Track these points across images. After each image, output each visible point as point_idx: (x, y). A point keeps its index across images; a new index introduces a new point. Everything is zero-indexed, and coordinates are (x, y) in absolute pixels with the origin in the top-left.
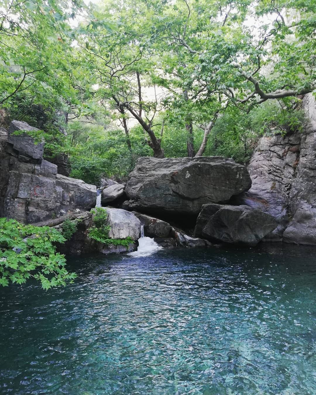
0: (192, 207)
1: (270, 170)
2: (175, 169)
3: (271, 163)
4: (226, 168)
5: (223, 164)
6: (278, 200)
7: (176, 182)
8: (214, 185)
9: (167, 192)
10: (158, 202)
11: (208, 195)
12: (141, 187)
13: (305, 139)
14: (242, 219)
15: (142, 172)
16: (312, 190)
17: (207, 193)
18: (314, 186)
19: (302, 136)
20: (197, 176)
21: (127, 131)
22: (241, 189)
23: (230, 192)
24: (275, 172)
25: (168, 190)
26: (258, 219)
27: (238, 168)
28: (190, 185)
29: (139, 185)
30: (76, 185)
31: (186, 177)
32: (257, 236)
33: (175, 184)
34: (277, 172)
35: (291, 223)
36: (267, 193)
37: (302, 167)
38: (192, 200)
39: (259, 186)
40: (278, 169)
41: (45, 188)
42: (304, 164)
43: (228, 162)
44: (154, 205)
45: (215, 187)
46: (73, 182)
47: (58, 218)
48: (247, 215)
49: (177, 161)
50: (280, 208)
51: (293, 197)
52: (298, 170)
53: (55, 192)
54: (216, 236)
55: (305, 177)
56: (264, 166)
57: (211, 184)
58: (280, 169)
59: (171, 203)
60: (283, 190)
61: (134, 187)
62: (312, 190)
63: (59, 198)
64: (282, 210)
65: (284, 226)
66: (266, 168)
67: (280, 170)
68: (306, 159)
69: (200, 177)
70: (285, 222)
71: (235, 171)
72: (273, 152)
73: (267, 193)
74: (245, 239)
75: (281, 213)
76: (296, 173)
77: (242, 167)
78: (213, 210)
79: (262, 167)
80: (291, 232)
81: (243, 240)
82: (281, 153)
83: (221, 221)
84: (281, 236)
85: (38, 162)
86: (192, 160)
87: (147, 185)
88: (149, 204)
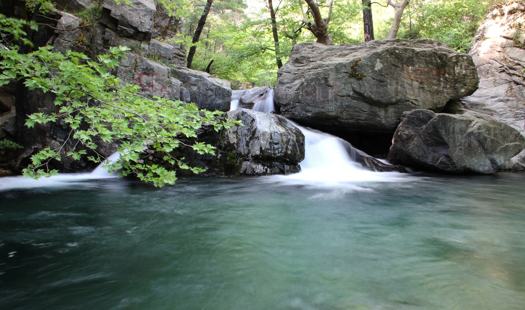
0: (385, 117)
2: (355, 57)
4: (440, 57)
5: (434, 49)
6: (518, 111)
7: (359, 78)
12: (302, 84)
15: (302, 65)
22: (463, 91)
24: (511, 68)
31: (376, 69)
34: (514, 69)
38: (385, 105)
39: (484, 91)
41: (155, 77)
43: (441, 47)
44: (324, 112)
45: (421, 86)
48: (480, 126)
49: (359, 46)
54: (429, 160)
61: (288, 85)
67: (520, 65)
69: (398, 69)
73: (501, 101)
74: (475, 165)
85: (146, 37)
87: (312, 80)
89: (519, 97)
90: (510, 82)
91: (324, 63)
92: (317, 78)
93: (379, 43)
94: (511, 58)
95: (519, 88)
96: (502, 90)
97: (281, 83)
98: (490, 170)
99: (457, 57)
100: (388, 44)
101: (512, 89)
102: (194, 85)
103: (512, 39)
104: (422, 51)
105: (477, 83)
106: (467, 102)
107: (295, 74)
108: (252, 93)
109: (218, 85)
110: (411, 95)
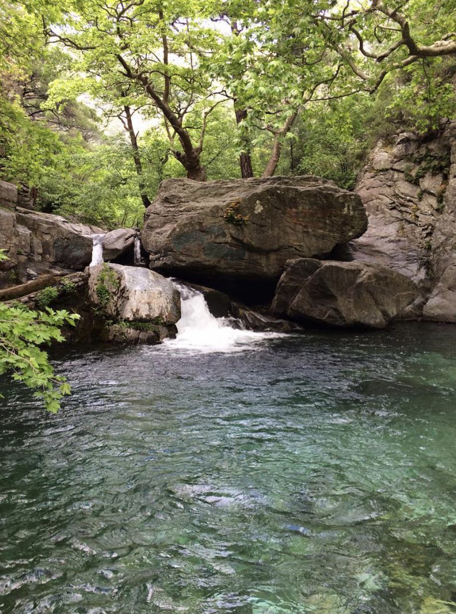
0: (267, 265)
1: (394, 203)
2: (232, 198)
4: (327, 197)
5: (320, 189)
6: (410, 253)
8: (305, 227)
12: (174, 230)
14: (361, 283)
15: (172, 205)
24: (403, 205)
25: (224, 235)
26: (385, 281)
29: (168, 228)
30: (53, 223)
31: (256, 212)
32: (385, 313)
35: (435, 292)
36: (391, 241)
40: (410, 201)
43: (326, 185)
45: (305, 230)
46: (47, 218)
50: (414, 267)
53: (17, 235)
54: (315, 314)
58: (412, 199)
61: (158, 230)
64: (419, 270)
66: (387, 200)
70: (426, 290)
71: (341, 200)
72: (398, 171)
73: (391, 241)
76: (443, 207)
79: (377, 198)
80: (437, 306)
81: (362, 321)
87: (185, 225)
89: (412, 237)
90: (402, 220)
91: (197, 205)
93: (258, 182)
94: (402, 194)
95: (412, 227)
96: (392, 230)
99: (345, 196)
101: (403, 228)
102: (46, 234)
103: (402, 172)
105: (367, 223)
108: (115, 236)
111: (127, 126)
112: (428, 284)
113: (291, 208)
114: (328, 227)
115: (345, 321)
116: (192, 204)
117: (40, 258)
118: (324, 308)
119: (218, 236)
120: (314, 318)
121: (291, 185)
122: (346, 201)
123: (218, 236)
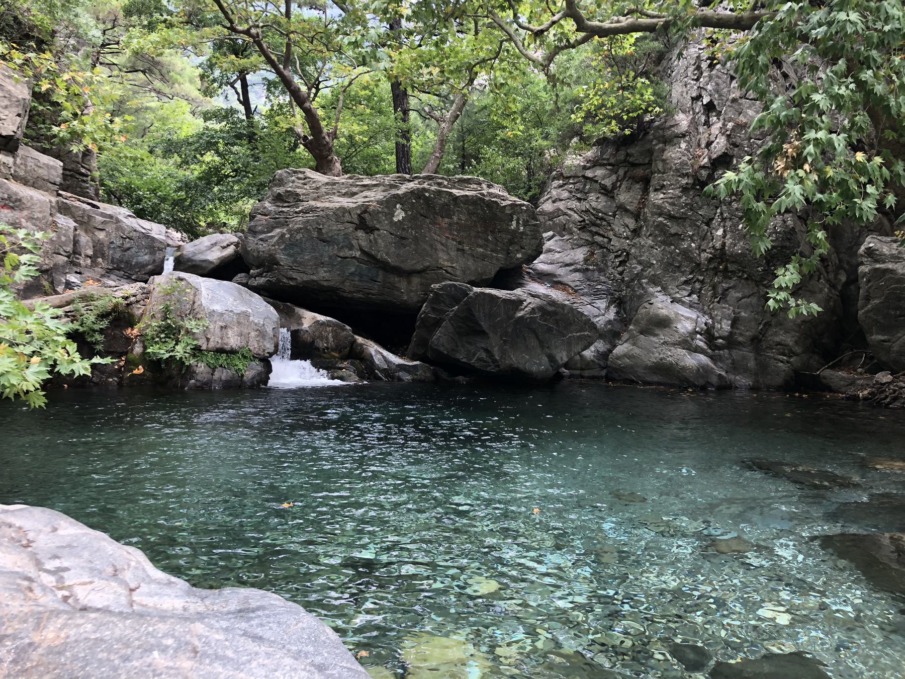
0: (407, 291)
1: (584, 221)
3: (584, 205)
6: (599, 287)
9: (347, 253)
10: (323, 275)
11: (446, 263)
12: (283, 235)
13: (663, 150)
16: (672, 265)
17: (443, 259)
18: (678, 255)
19: (656, 145)
20: (421, 218)
21: (249, 112)
22: (519, 256)
23: (494, 262)
24: (594, 224)
27: (514, 205)
28: (404, 238)
30: (111, 217)
31: (395, 219)
32: (552, 359)
33: (367, 233)
35: (625, 336)
37: (653, 214)
38: (408, 274)
39: (557, 255)
40: (602, 219)
42: (659, 207)
43: (491, 190)
44: (314, 281)
45: (460, 247)
47: (57, 293)
50: (602, 304)
51: (633, 280)
52: (645, 220)
54: (461, 357)
55: (660, 235)
56: (569, 212)
57: (453, 239)
58: (605, 217)
59: (357, 278)
60: (609, 264)
62: (672, 265)
63: (65, 244)
64: (608, 308)
65: (610, 343)
67: (605, 220)
68: (662, 196)
69: (428, 221)
70: (612, 335)
73: (576, 270)
75: (603, 315)
76: (641, 227)
77: (524, 205)
78: (458, 296)
80: (626, 355)
81: (521, 367)
82: (608, 182)
83: (470, 327)
84: (602, 363)
86: (409, 181)
87: (298, 231)
88: (300, 277)
92: (306, 228)
94: (594, 209)
95: (603, 252)
97: (253, 231)
98: (547, 369)
100: (416, 182)
104: (463, 196)
106: (533, 270)
107: (275, 218)
108: (208, 244)
109: (143, 231)
110: (444, 260)
111: (241, 99)
112: (617, 327)
113: (442, 217)
114: (490, 245)
115: (498, 366)
116: (312, 203)
117: (89, 261)
118: (472, 348)
119: (342, 247)
120: (459, 360)
121: (445, 187)
122: (514, 213)
123: (342, 247)
